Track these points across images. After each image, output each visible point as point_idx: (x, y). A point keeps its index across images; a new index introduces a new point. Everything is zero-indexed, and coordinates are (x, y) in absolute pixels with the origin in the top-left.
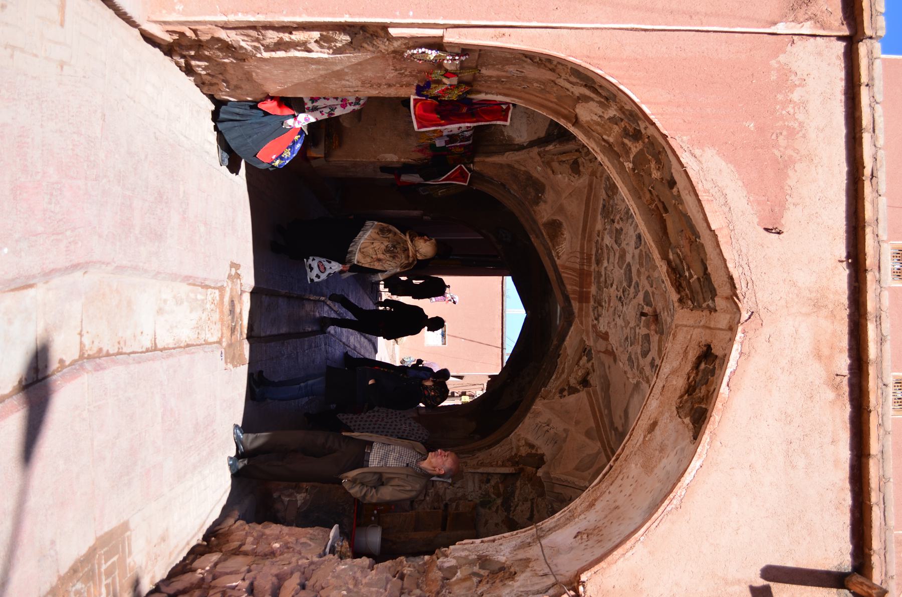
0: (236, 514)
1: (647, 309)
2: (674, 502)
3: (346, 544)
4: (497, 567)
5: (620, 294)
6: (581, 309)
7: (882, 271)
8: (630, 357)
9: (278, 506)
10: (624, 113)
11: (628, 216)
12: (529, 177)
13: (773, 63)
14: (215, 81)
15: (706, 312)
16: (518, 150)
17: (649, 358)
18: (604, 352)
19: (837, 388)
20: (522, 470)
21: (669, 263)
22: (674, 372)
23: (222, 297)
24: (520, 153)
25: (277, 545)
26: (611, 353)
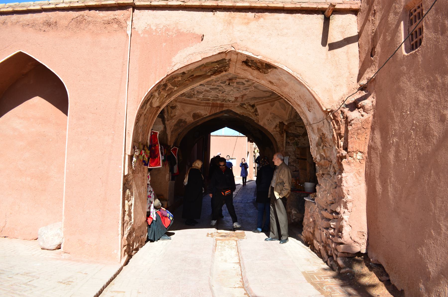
0: (299, 235)
1: (227, 83)
2: (298, 76)
3: (311, 195)
4: (320, 140)
5: (221, 92)
6: (226, 107)
8: (244, 89)
9: (296, 220)
10: (157, 90)
11: (193, 89)
12: (176, 125)
13: (141, 36)
14: (140, 240)
15: (231, 62)
17: (245, 82)
19: (259, 17)
20: (285, 130)
21: (212, 75)
22: (252, 74)
23: (219, 240)
25: (311, 220)
26: (243, 96)
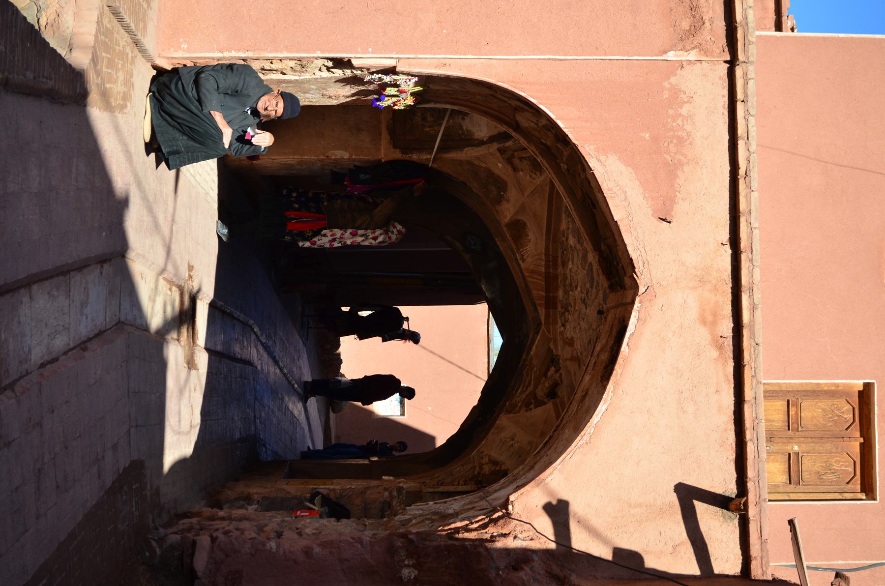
2: (585, 438)
6: (547, 316)
7: (754, 252)
12: (490, 174)
13: (666, 84)
18: (571, 359)
19: (720, 348)
24: (479, 148)
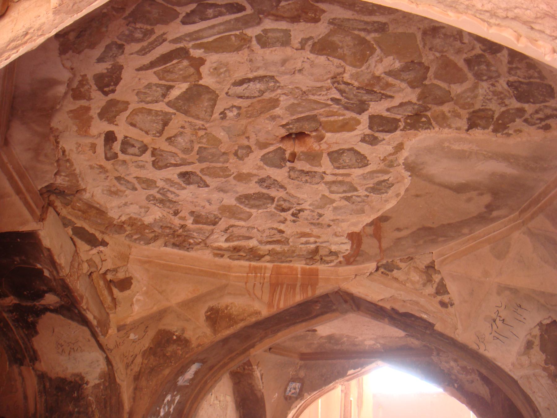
5: (288, 215)
16: (112, 365)
18: (379, 241)
